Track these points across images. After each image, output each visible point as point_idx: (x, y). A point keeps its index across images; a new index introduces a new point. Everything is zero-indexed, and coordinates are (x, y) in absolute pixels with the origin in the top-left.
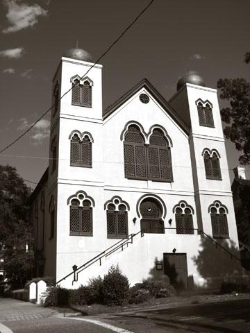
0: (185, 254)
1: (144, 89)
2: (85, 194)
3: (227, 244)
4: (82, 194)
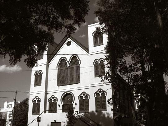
0: (61, 122)
1: (69, 38)
2: (86, 93)
3: (104, 115)
4: (84, 93)
